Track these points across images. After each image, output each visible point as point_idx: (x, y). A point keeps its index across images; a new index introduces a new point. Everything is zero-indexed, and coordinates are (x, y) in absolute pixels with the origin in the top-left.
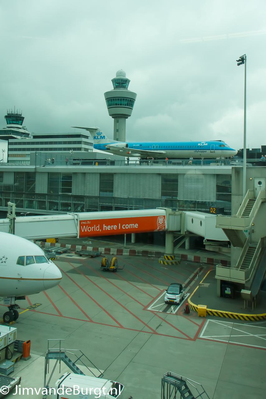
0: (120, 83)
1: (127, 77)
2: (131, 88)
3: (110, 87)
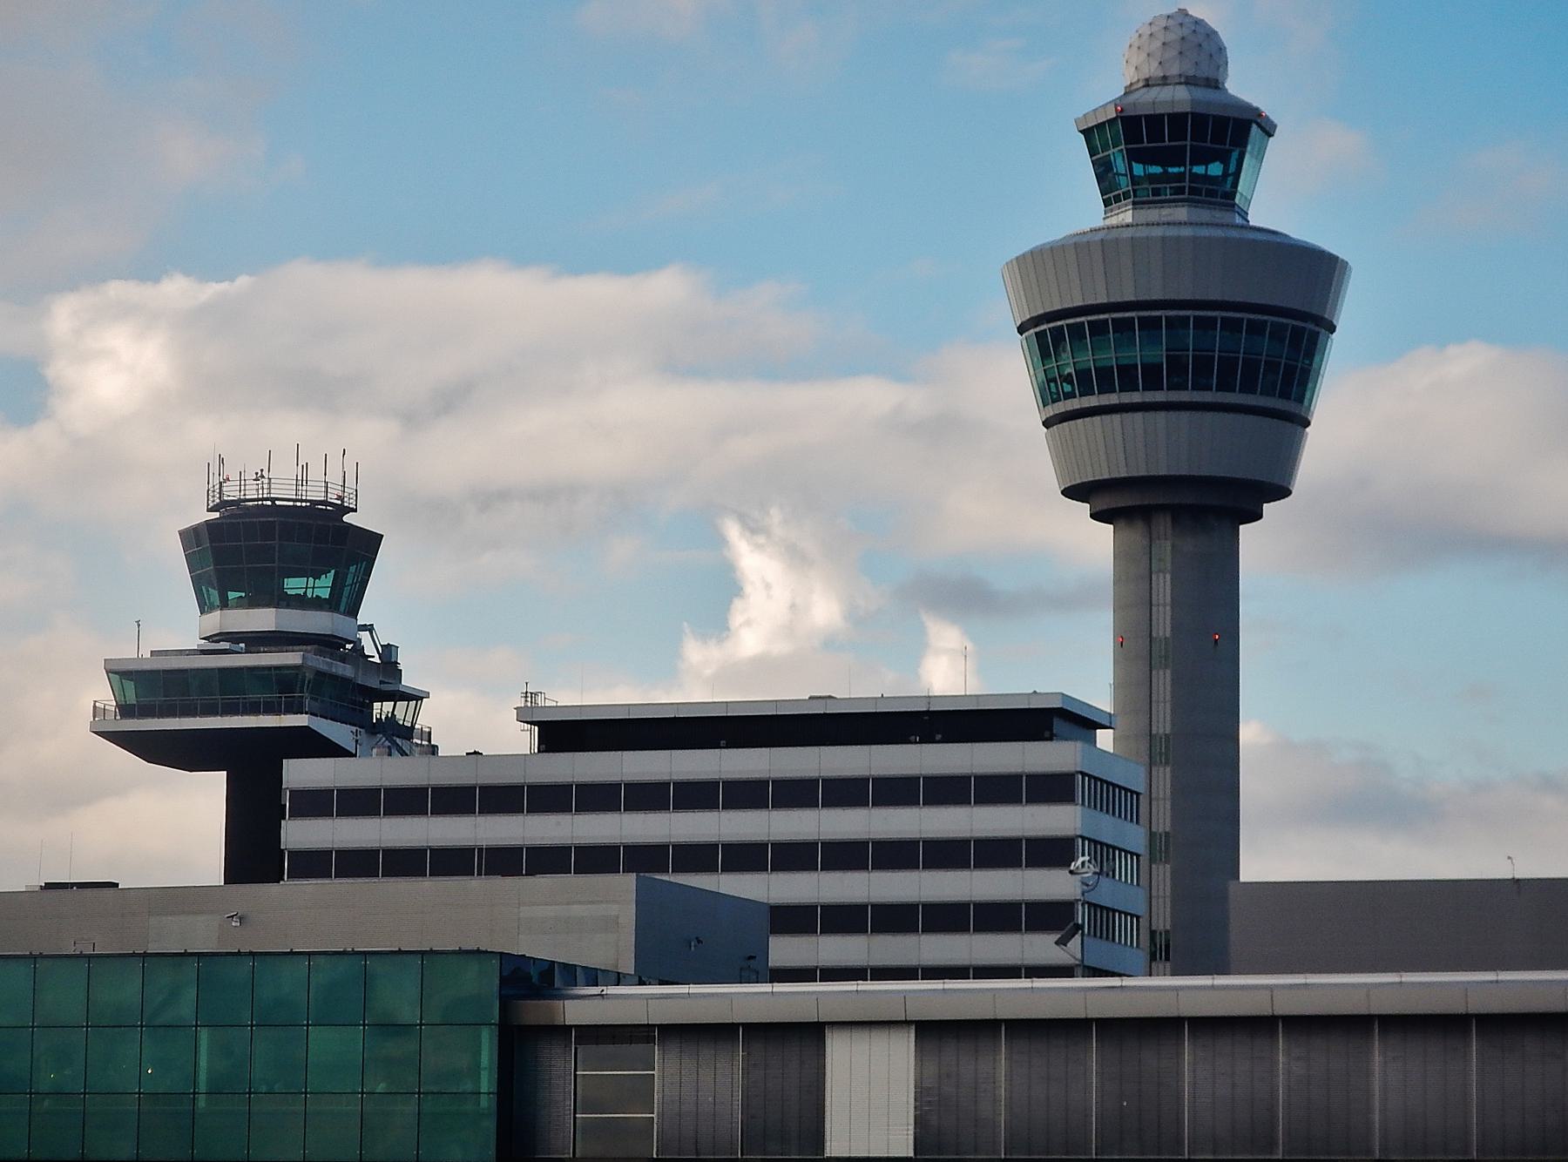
0: (1179, 142)
1: (1243, 84)
2: (1280, 195)
3: (1074, 204)
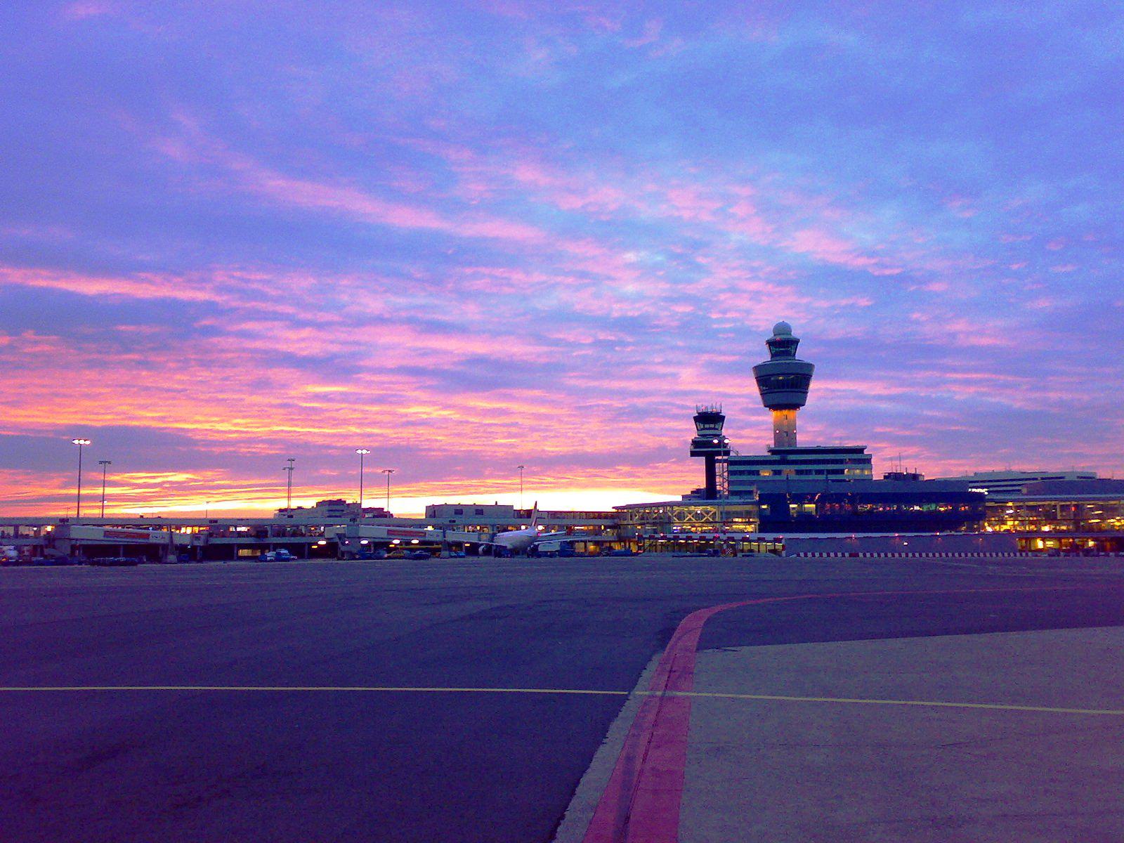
2: (802, 354)
3: (765, 357)
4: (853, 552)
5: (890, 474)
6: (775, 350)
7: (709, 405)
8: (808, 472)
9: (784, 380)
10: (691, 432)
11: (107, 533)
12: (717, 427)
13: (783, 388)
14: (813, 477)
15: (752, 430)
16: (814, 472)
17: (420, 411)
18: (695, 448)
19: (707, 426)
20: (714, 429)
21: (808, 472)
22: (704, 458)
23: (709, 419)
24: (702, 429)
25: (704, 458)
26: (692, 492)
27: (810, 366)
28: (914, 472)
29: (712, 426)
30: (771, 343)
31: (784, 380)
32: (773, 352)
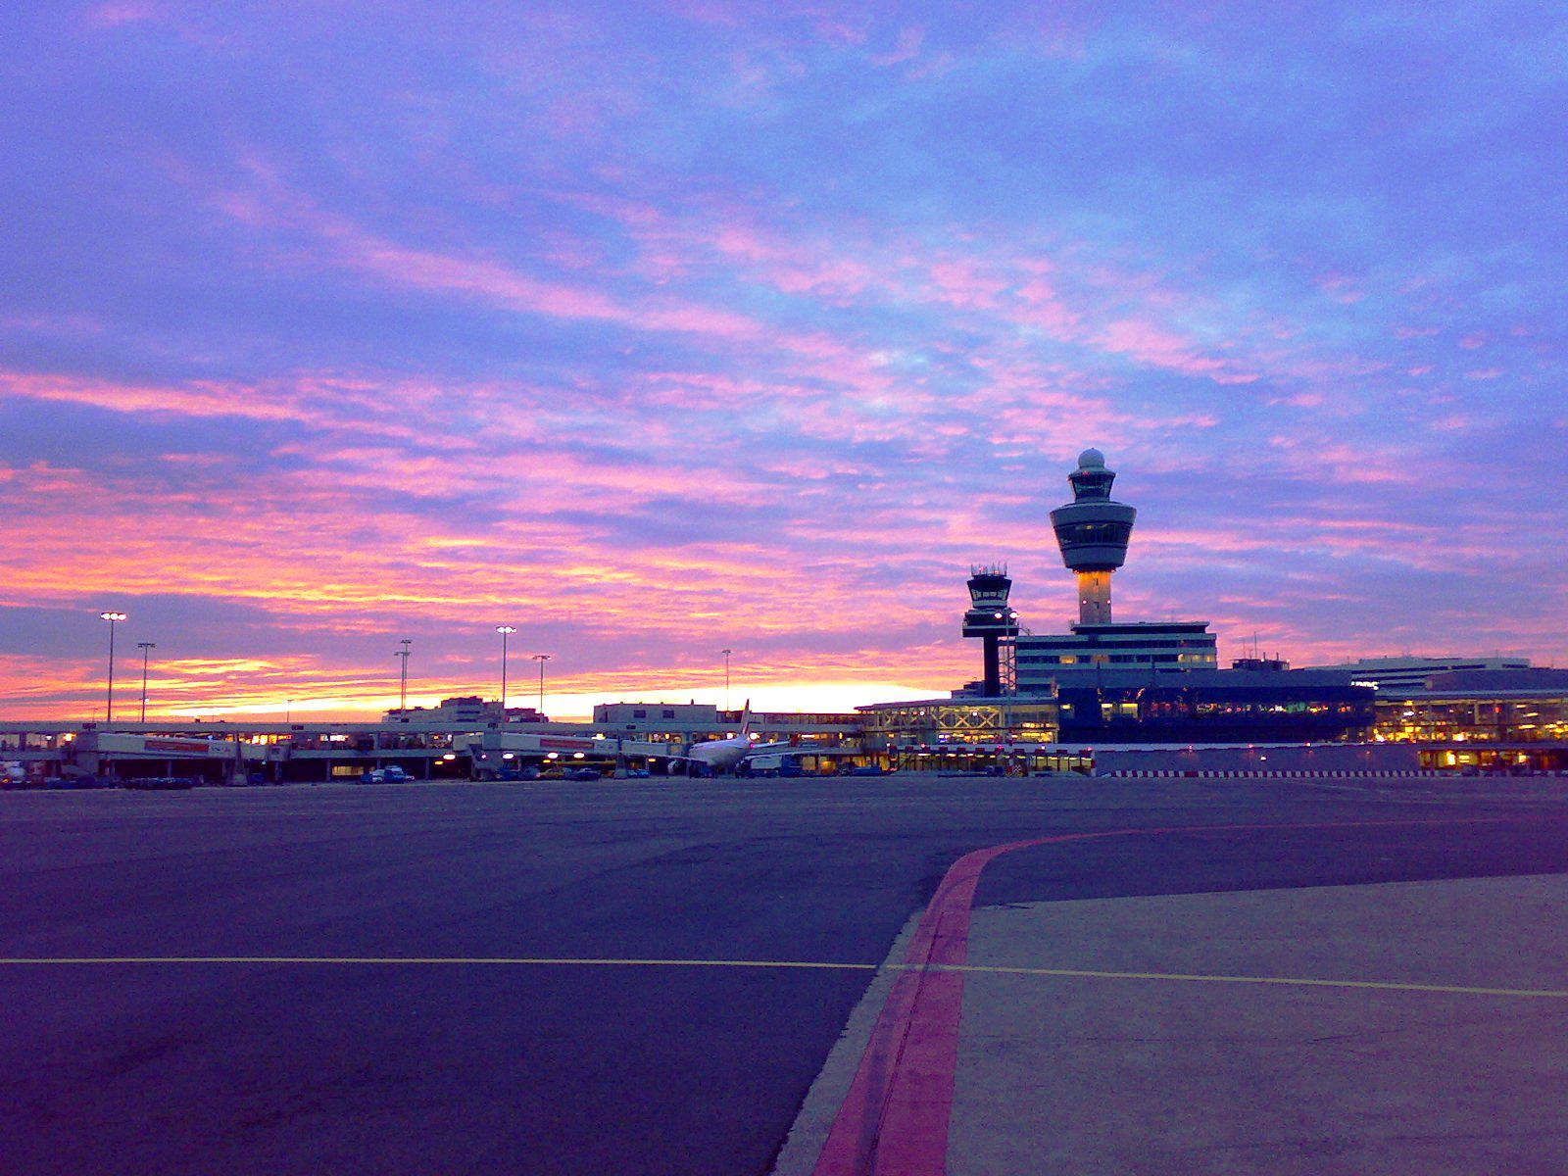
2: (1118, 494)
3: (1067, 498)
4: (1190, 770)
5: (1241, 661)
6: (1081, 488)
7: (989, 565)
8: (1128, 659)
9: (1093, 530)
10: (964, 603)
11: (149, 744)
12: (1000, 596)
13: (1093, 541)
14: (1134, 665)
15: (1049, 600)
16: (1135, 659)
17: (585, 573)
18: (969, 625)
19: (986, 594)
20: (997, 598)
21: (1128, 659)
22: (982, 639)
23: (989, 585)
24: (979, 599)
25: (982, 639)
26: (966, 687)
27: (1130, 511)
28: (1274, 659)
29: (993, 594)
30: (1075, 479)
31: (1093, 530)
32: (1078, 491)
